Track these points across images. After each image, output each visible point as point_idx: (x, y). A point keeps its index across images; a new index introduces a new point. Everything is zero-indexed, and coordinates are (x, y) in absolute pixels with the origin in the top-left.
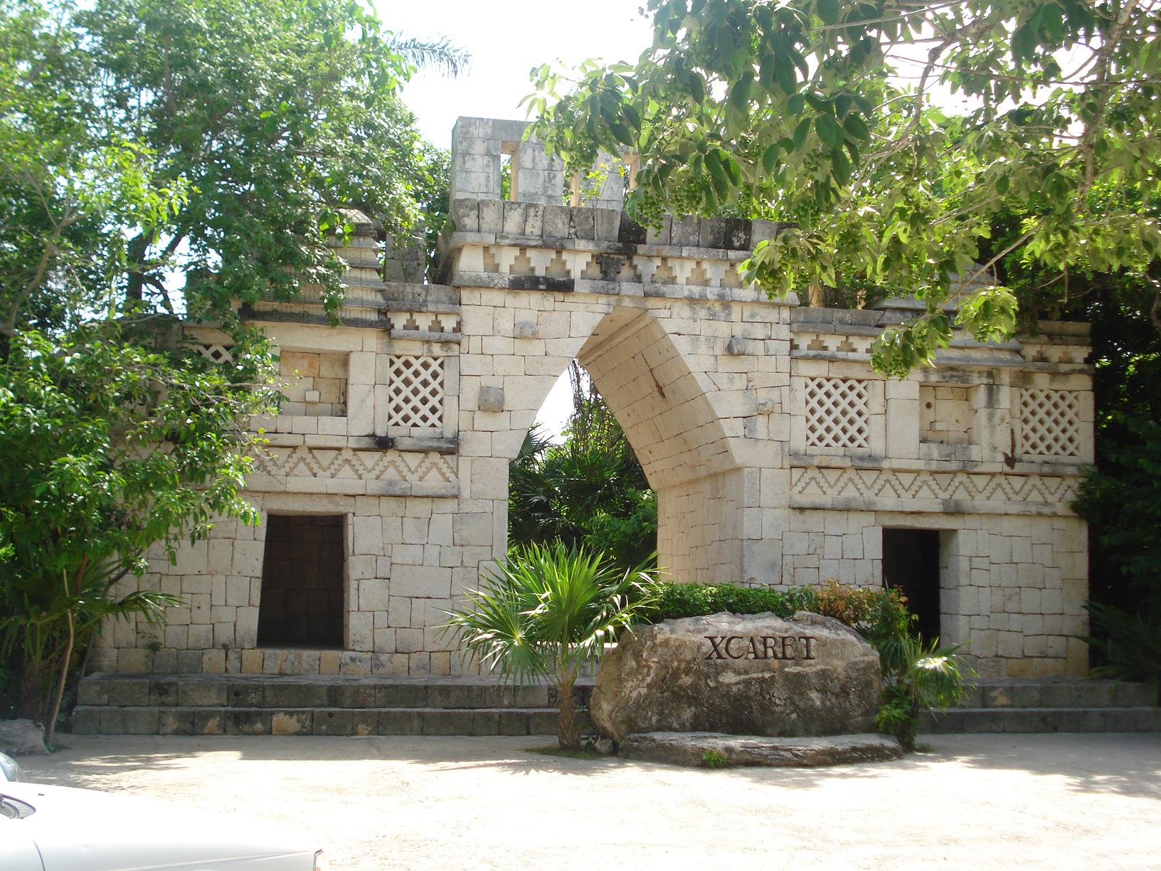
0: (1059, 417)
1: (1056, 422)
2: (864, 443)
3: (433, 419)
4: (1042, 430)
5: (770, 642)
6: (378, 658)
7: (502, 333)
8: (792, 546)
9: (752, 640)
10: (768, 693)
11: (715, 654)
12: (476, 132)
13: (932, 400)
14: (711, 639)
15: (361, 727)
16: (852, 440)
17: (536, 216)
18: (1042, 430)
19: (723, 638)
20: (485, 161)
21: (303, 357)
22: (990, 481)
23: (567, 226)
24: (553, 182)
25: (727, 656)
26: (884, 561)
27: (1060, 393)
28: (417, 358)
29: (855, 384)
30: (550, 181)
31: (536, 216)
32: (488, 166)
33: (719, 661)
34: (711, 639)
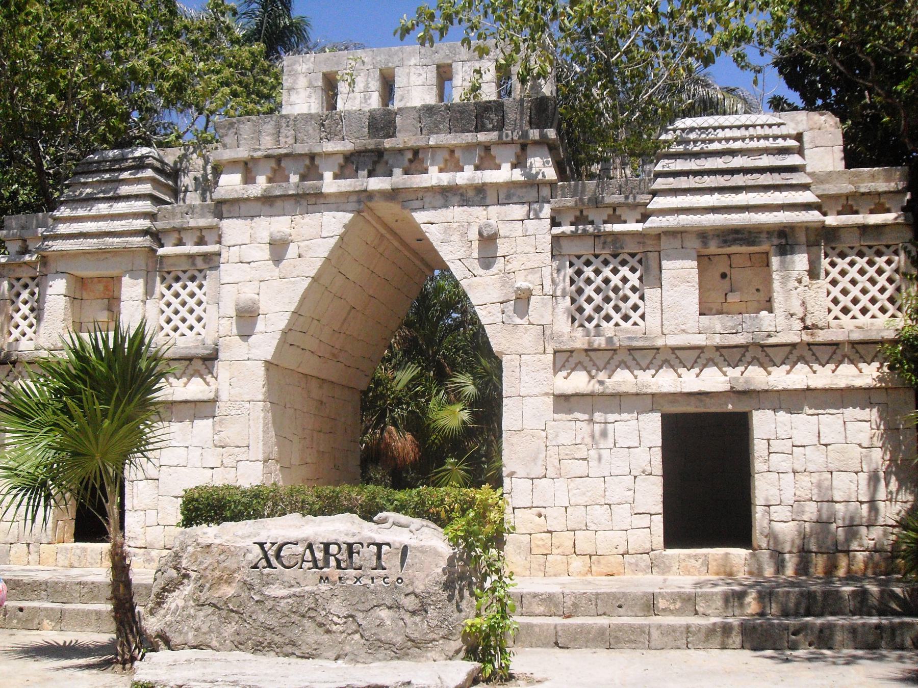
0: (876, 276)
1: (873, 281)
2: (640, 321)
3: (198, 327)
4: (855, 291)
5: (333, 549)
6: (149, 554)
7: (259, 240)
8: (557, 436)
9: (310, 547)
10: (324, 609)
11: (264, 563)
12: (300, 68)
13: (727, 271)
14: (261, 545)
15: (46, 622)
16: (626, 318)
17: (288, 126)
18: (855, 291)
19: (273, 544)
20: (308, 93)
21: (99, 282)
22: (791, 353)
23: (318, 131)
24: (369, 102)
25: (279, 566)
26: (665, 448)
27: (874, 249)
28: (185, 272)
29: (628, 258)
30: (366, 102)
31: (288, 126)
32: (310, 97)
33: (267, 570)
34: (261, 545)
